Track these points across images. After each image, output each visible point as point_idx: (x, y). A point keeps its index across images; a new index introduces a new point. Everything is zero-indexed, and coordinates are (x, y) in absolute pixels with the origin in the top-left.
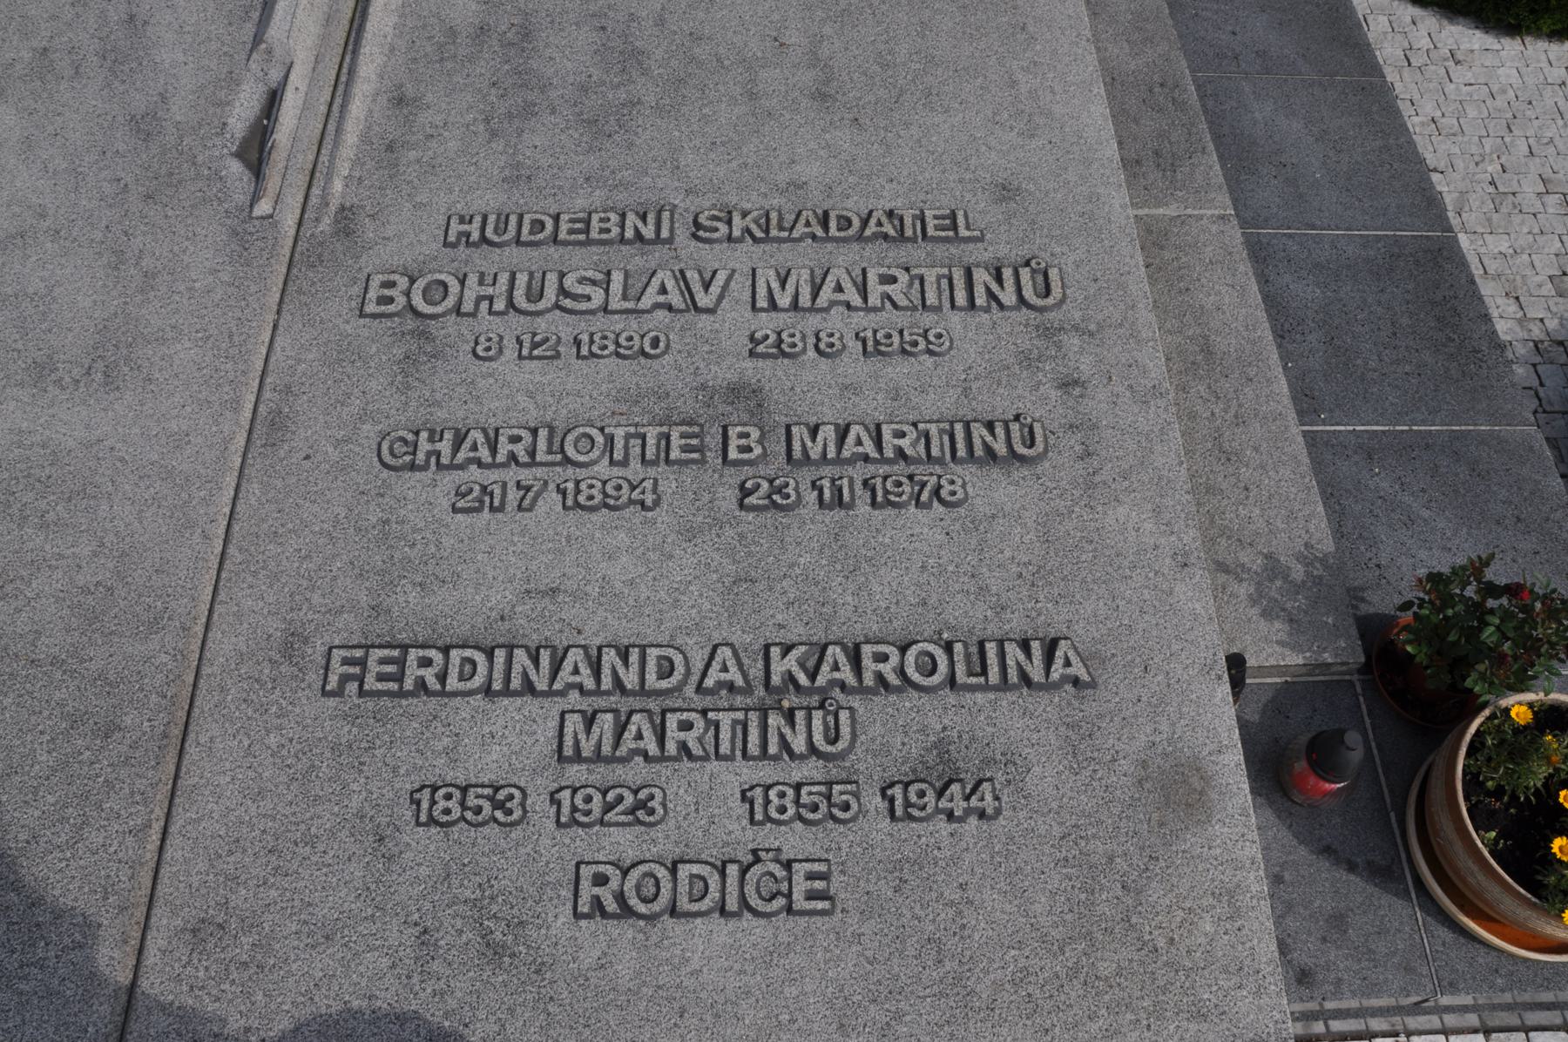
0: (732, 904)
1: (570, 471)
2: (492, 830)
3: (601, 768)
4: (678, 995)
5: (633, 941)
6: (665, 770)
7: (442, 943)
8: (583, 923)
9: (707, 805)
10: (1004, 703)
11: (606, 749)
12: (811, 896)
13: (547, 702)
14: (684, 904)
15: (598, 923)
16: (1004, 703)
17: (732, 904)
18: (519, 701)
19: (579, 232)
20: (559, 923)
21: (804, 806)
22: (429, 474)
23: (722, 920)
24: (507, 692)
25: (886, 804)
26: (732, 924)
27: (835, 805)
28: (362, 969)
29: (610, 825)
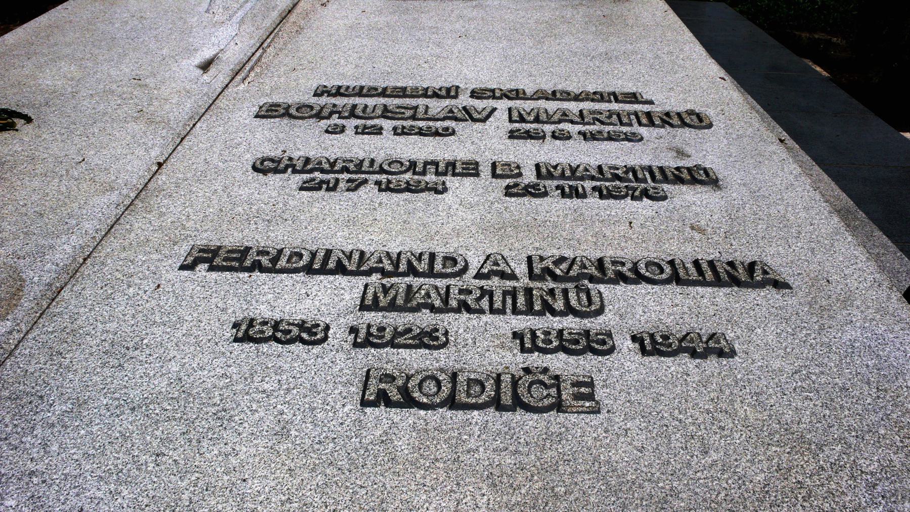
0: (507, 399)
1: (385, 176)
2: (297, 348)
3: (394, 314)
4: (454, 468)
5: (414, 427)
6: (449, 317)
7: (237, 418)
8: (368, 410)
9: (483, 344)
10: (721, 294)
11: (400, 301)
12: (578, 397)
13: (354, 280)
14: (462, 397)
15: (381, 411)
16: (721, 294)
17: (507, 399)
18: (331, 278)
19: (234, 259)
20: (346, 409)
21: (566, 340)
22: (286, 175)
23: (497, 413)
24: (323, 271)
25: (637, 345)
26: (507, 415)
27: (593, 341)
28: (158, 433)
29: (399, 346)
